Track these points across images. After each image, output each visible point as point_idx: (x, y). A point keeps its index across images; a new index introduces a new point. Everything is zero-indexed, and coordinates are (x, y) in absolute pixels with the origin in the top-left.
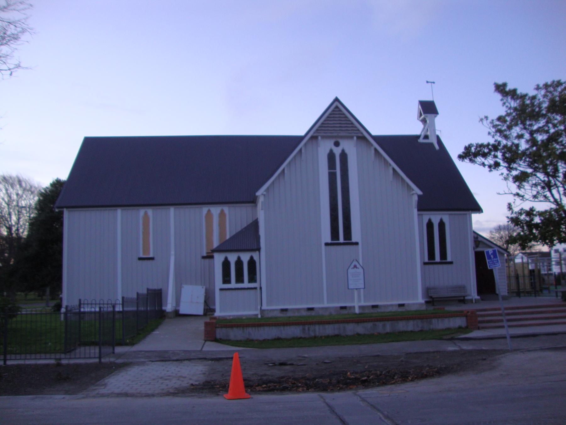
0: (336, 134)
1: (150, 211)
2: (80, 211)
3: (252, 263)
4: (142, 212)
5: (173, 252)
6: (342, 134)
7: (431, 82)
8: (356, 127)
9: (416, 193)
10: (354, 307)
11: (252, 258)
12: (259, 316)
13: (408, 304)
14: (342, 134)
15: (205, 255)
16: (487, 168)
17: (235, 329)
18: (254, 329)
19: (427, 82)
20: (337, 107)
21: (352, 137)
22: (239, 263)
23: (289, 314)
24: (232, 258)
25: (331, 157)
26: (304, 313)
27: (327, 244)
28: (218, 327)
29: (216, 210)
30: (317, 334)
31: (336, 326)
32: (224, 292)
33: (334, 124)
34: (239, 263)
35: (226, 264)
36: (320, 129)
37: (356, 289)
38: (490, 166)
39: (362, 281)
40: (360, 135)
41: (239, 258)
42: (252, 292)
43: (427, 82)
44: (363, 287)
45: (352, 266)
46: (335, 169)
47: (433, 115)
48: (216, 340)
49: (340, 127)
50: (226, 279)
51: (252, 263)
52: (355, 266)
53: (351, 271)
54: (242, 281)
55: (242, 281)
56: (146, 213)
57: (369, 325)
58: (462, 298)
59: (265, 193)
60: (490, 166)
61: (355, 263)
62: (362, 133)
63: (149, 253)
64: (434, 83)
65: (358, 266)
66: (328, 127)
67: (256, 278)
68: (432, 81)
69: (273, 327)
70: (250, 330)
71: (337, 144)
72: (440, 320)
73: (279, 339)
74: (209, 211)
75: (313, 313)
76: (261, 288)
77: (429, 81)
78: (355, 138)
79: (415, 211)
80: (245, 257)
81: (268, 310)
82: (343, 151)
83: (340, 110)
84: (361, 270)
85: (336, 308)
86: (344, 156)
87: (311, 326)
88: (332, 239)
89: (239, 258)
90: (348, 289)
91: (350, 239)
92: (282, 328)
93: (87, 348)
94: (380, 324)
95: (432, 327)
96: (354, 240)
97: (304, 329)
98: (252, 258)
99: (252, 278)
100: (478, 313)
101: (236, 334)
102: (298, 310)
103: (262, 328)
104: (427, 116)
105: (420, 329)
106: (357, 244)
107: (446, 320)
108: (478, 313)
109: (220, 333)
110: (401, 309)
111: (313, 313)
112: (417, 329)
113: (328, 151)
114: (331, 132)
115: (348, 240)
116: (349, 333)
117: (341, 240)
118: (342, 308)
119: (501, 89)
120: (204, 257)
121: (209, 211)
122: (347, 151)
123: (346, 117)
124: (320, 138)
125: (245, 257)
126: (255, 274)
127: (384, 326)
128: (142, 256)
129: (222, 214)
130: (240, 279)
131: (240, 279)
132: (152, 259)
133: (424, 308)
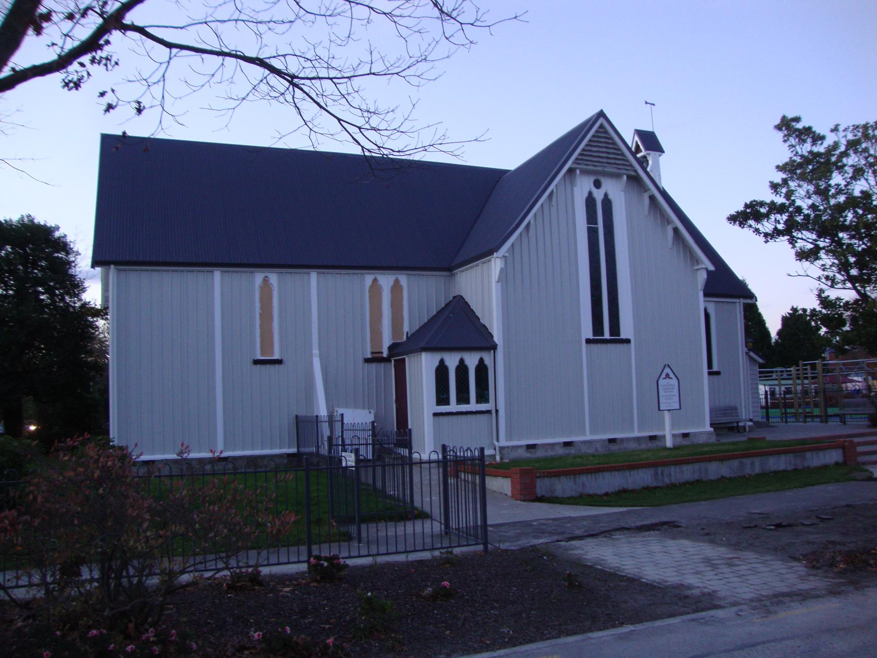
0: (600, 169)
1: (274, 278)
2: (152, 270)
3: (482, 369)
4: (259, 277)
5: (316, 351)
6: (609, 169)
7: (651, 104)
8: (627, 161)
9: (707, 269)
10: (664, 437)
11: (481, 361)
12: (498, 458)
13: (695, 434)
14: (609, 169)
15: (369, 356)
16: (761, 239)
17: (563, 478)
18: (589, 476)
19: (646, 103)
20: (601, 126)
21: (618, 176)
22: (462, 369)
23: (540, 454)
24: (452, 361)
25: (590, 201)
26: (561, 451)
27: (588, 341)
28: (539, 477)
29: (386, 280)
30: (673, 480)
31: (696, 466)
32: (441, 418)
33: (598, 151)
34: (462, 369)
35: (441, 372)
36: (581, 157)
37: (669, 410)
38: (766, 235)
39: (676, 399)
40: (633, 173)
41: (462, 361)
42: (484, 417)
43: (646, 103)
44: (679, 408)
45: (663, 375)
46: (596, 223)
47: (658, 153)
48: (541, 499)
49: (607, 158)
50: (442, 398)
51: (482, 369)
52: (667, 376)
53: (661, 382)
54: (467, 401)
55: (467, 401)
56: (266, 280)
57: (735, 463)
58: (735, 425)
59: (507, 254)
60: (766, 235)
61: (667, 370)
62: (636, 171)
63: (272, 353)
64: (654, 105)
65: (671, 375)
66: (591, 156)
67: (488, 395)
68: (652, 103)
69: (616, 473)
70: (583, 478)
71: (597, 184)
72: (814, 453)
73: (625, 491)
74: (375, 280)
75: (572, 451)
76: (497, 411)
77: (648, 102)
78: (625, 177)
79: (701, 294)
80: (472, 360)
81: (508, 447)
82: (606, 195)
83: (606, 132)
84: (674, 381)
85: (603, 441)
86: (607, 203)
87: (666, 468)
88: (594, 334)
89: (462, 361)
90: (659, 410)
91: (619, 335)
92: (627, 473)
93: (382, 525)
94: (747, 461)
95: (806, 464)
96: (623, 336)
97: (656, 474)
98: (481, 361)
99: (482, 397)
100: (856, 440)
101: (564, 486)
102: (552, 445)
103: (601, 474)
104: (649, 154)
105: (793, 467)
106: (628, 341)
107: (821, 454)
108: (856, 440)
109: (542, 486)
110: (685, 442)
111: (572, 451)
112: (790, 468)
113: (586, 195)
114: (586, 163)
115: (617, 339)
116: (713, 477)
117: (607, 335)
118: (612, 441)
119: (787, 125)
120: (367, 361)
121: (375, 280)
122: (611, 196)
123: (614, 143)
124: (578, 172)
125: (472, 360)
126: (487, 388)
127: (753, 463)
128: (259, 357)
129: (396, 288)
130: (463, 398)
131: (463, 398)
132: (279, 362)
133: (713, 439)
